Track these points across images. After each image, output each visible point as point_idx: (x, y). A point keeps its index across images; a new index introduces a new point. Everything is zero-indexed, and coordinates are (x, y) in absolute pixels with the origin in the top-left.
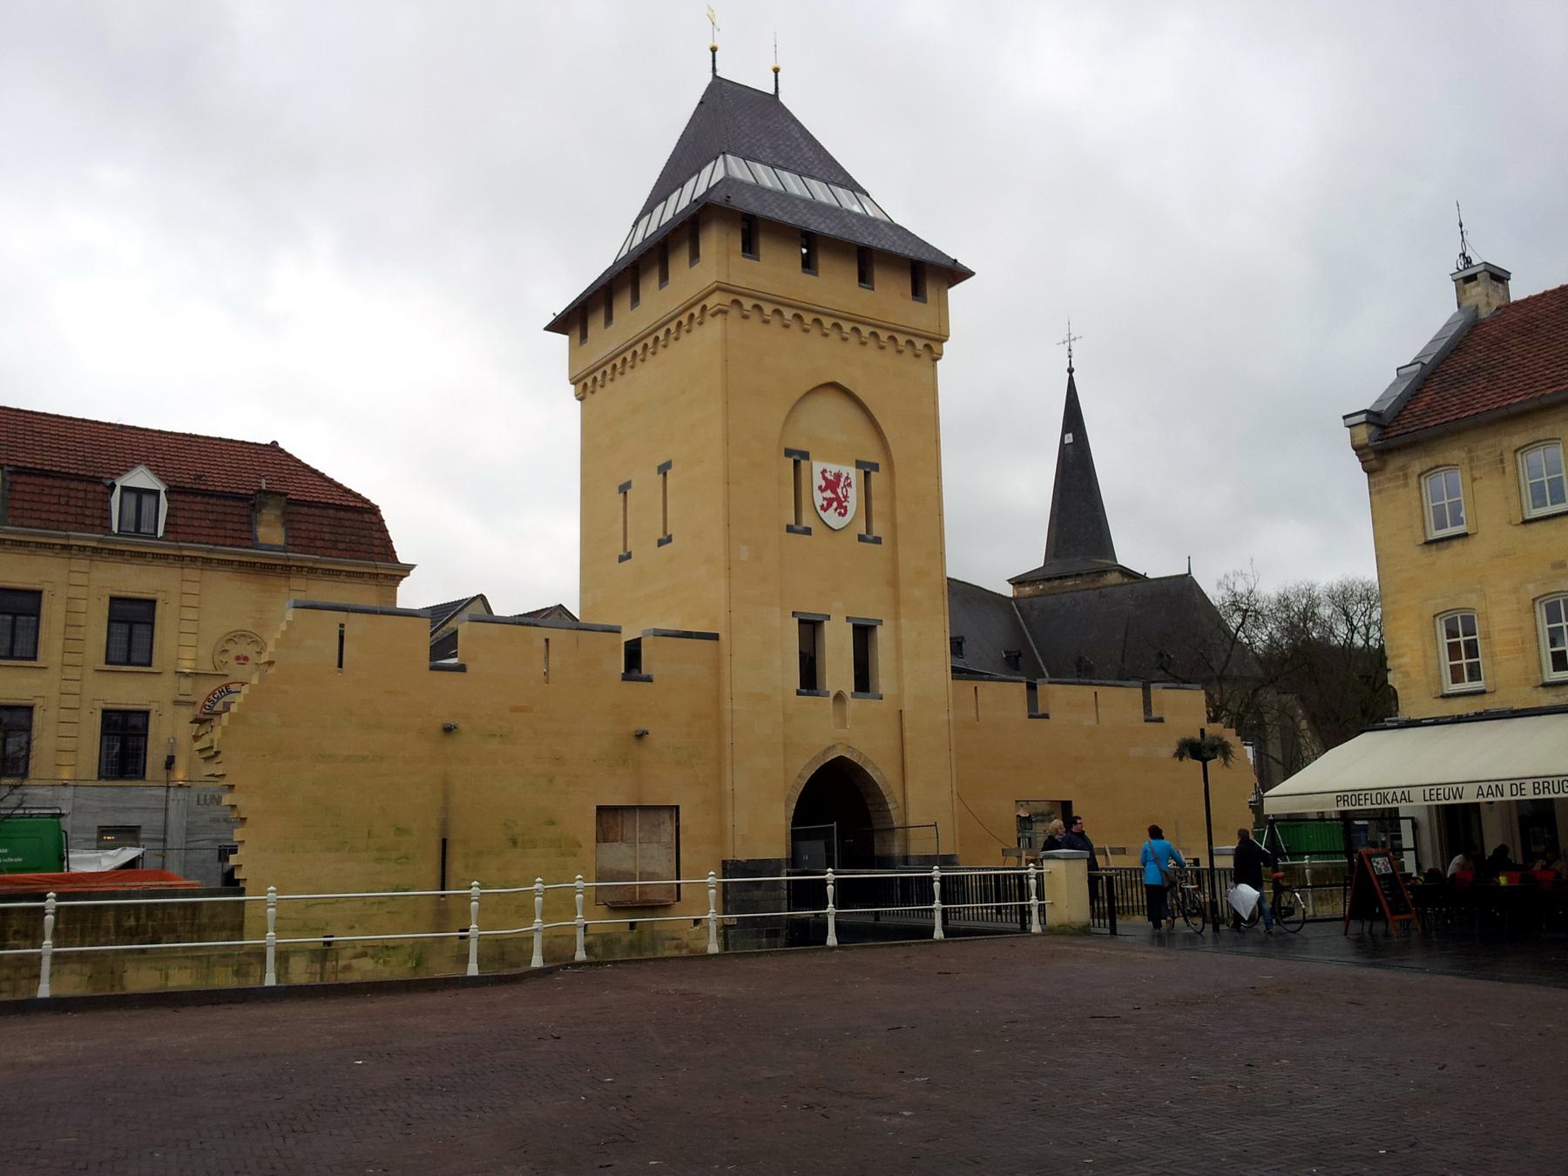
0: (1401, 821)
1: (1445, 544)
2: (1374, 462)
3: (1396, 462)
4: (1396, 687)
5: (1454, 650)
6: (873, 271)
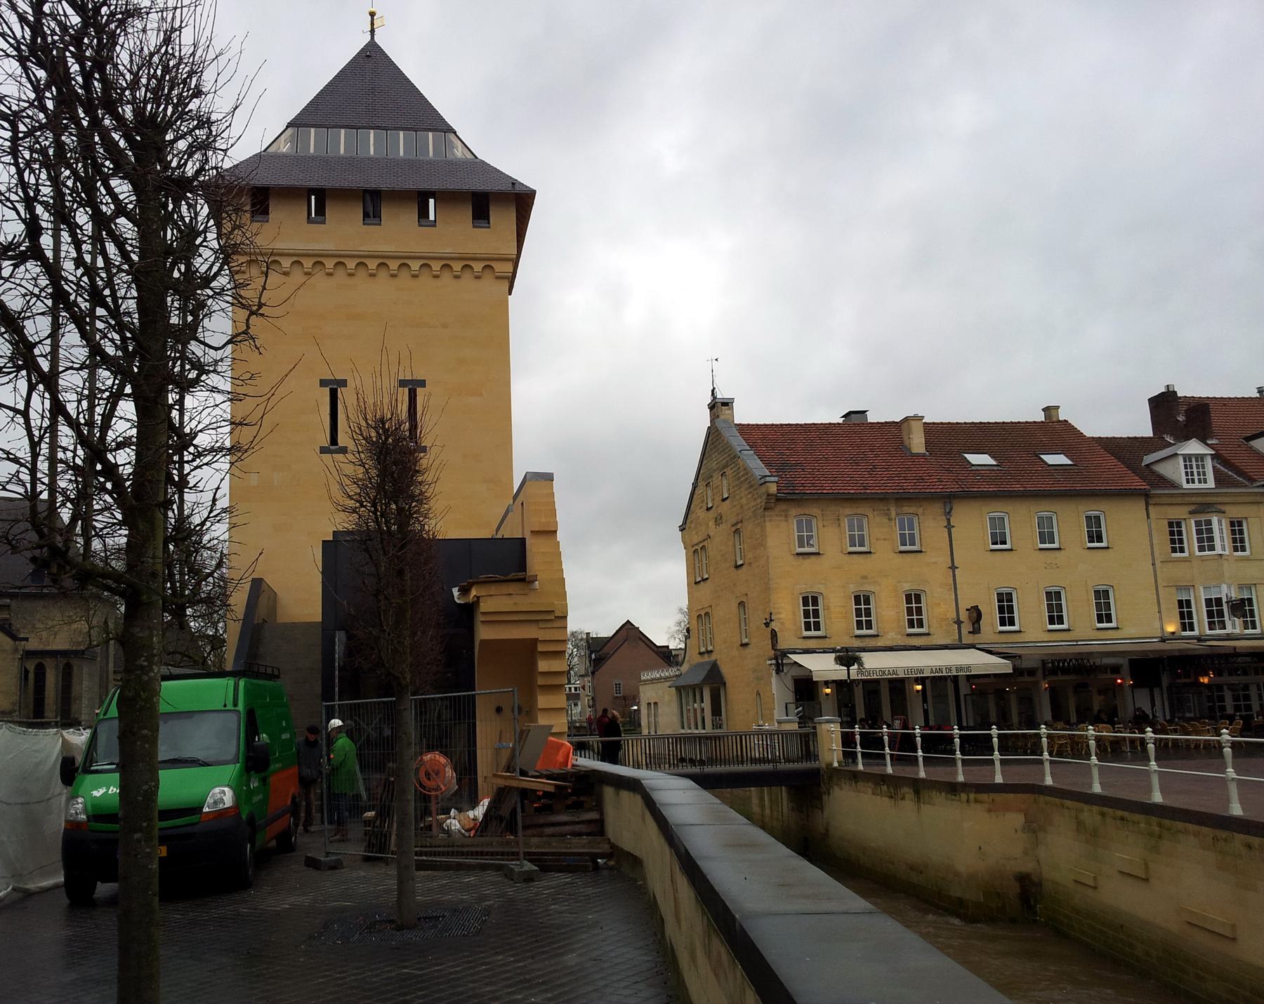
3: (782, 506)
5: (806, 614)
6: (536, 697)
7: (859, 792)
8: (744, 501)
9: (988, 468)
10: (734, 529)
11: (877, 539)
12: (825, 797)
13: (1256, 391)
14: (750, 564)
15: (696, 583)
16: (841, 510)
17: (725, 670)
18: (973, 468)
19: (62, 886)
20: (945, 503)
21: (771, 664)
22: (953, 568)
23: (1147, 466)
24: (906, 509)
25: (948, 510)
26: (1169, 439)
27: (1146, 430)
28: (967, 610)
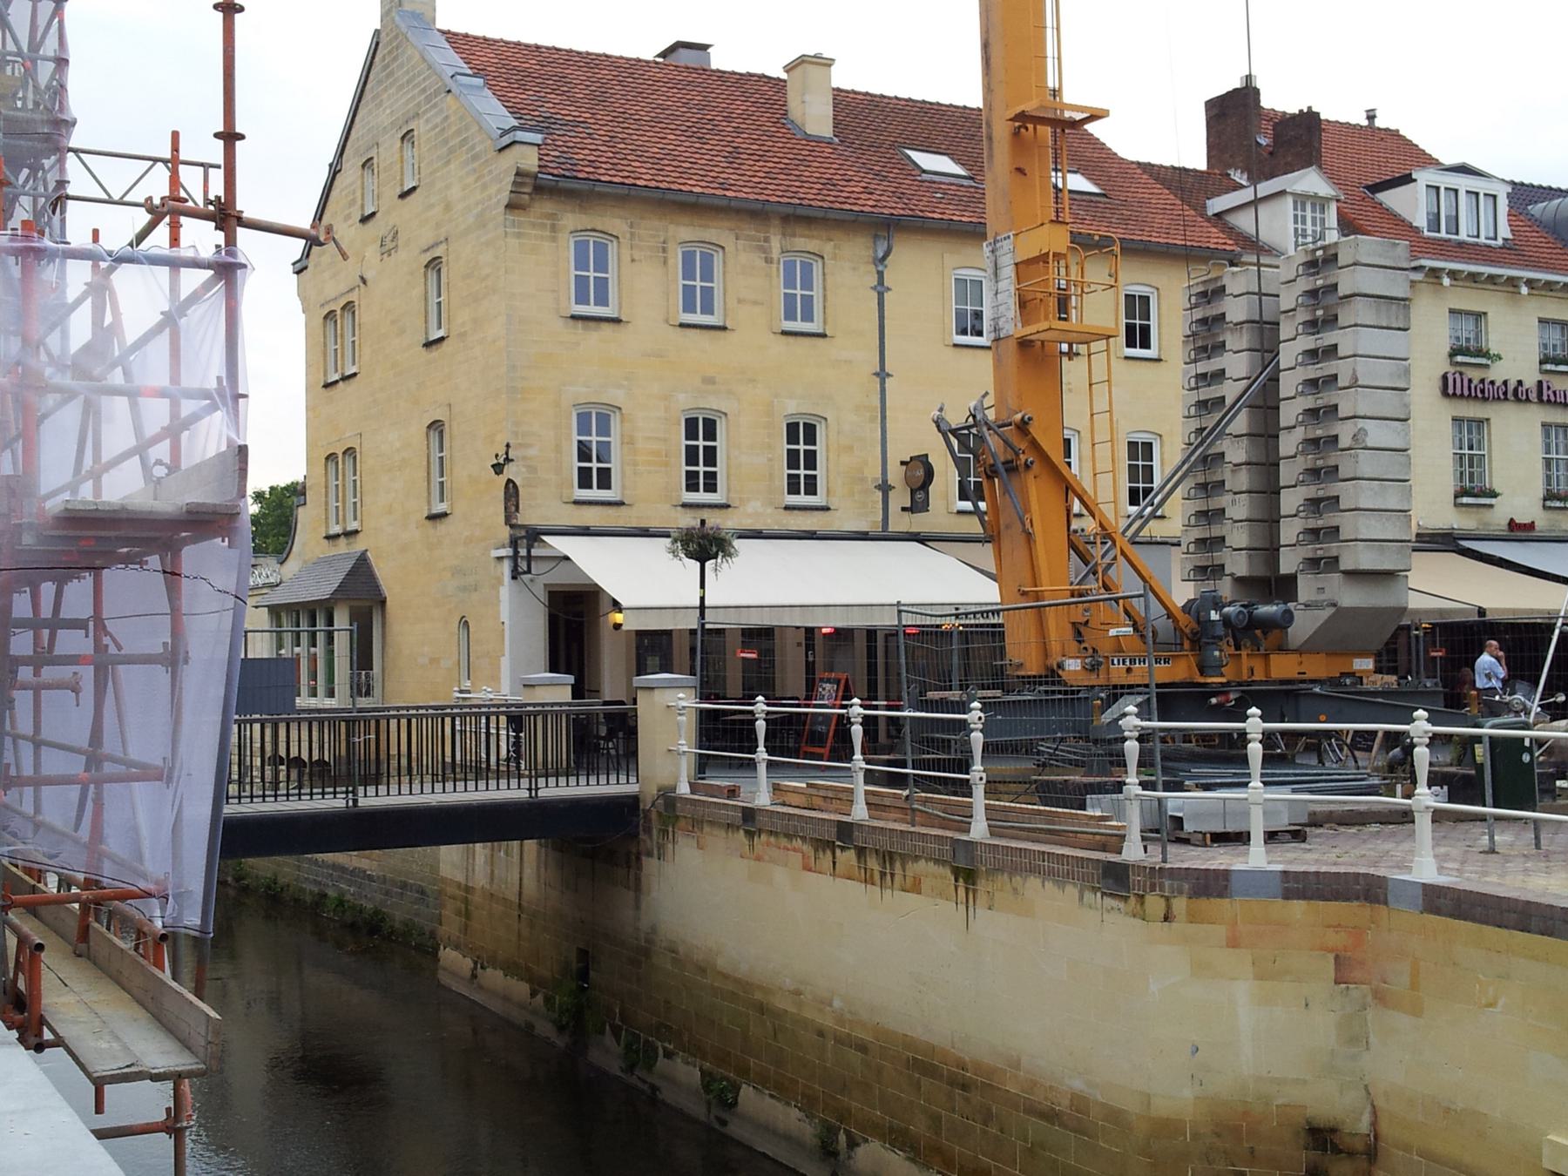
0: (249, 657)
1: (592, 324)
2: (526, 197)
3: (546, 206)
4: (518, 484)
7: (758, 859)
8: (455, 193)
9: (952, 180)
10: (428, 256)
11: (739, 301)
12: (650, 865)
13: (1365, 115)
14: (462, 335)
15: (327, 386)
16: (672, 228)
17: (384, 572)
18: (925, 176)
19: (1477, 339)
20: (876, 237)
21: (500, 559)
22: (882, 374)
23: (1218, 215)
24: (801, 243)
25: (881, 254)
26: (1238, 177)
27: (1195, 156)
28: (903, 463)
